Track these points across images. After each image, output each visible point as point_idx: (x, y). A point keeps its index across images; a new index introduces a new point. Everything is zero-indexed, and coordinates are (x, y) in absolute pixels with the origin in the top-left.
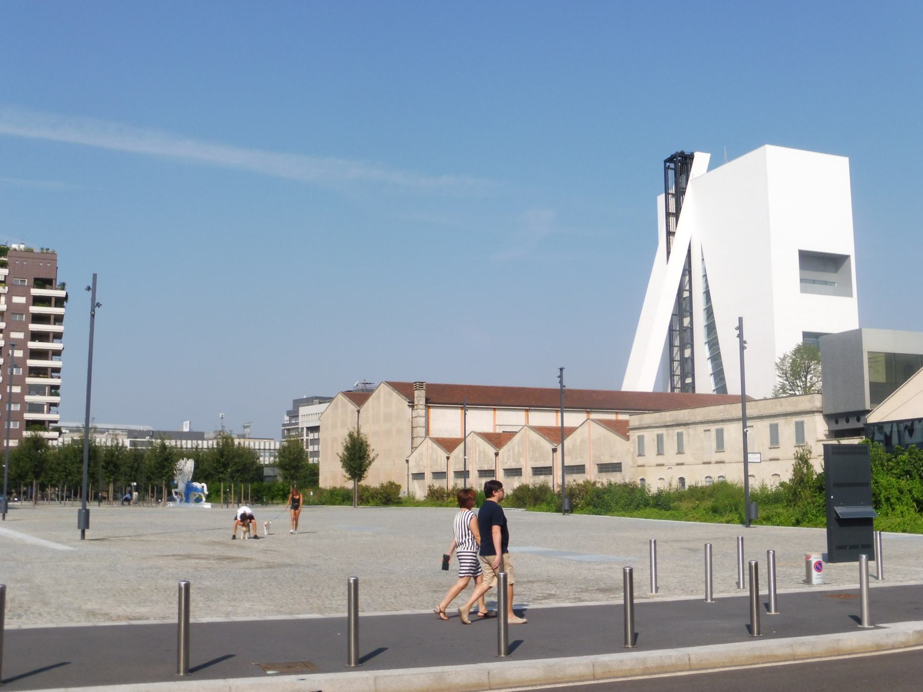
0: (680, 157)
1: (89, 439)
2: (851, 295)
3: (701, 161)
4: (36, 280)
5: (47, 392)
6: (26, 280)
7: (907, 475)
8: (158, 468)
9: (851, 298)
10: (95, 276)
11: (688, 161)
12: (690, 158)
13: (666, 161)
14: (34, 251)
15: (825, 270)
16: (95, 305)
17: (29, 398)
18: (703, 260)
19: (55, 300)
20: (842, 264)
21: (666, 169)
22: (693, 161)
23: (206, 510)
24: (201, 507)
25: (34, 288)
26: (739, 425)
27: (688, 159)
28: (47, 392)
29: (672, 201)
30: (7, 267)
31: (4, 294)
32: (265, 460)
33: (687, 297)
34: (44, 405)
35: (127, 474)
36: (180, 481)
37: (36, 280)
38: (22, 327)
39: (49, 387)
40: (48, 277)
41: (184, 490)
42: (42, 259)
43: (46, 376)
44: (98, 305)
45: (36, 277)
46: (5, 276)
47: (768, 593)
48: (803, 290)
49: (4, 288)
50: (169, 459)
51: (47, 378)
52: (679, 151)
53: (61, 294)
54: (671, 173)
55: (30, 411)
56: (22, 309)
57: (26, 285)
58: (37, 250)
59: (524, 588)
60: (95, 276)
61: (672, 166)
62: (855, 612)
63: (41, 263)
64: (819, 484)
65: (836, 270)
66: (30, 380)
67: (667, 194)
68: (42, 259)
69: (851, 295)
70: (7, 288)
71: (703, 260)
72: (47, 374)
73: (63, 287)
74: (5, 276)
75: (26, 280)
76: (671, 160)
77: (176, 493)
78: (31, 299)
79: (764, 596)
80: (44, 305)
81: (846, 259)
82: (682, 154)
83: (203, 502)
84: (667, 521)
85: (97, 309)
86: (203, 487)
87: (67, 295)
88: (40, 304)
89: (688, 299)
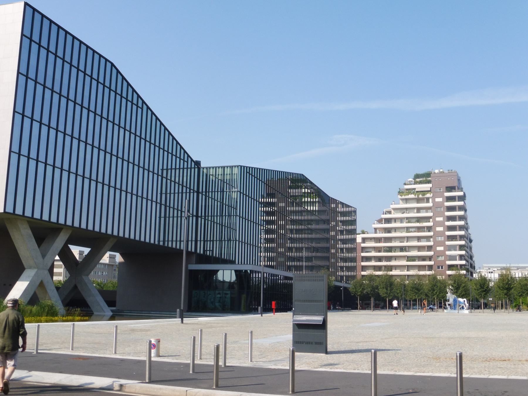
4: (447, 187)
5: (457, 249)
6: (442, 188)
7: (450, 280)
8: (430, 290)
14: (444, 172)
17: (448, 253)
19: (458, 197)
23: (466, 315)
24: (463, 312)
25: (446, 192)
28: (457, 249)
30: (431, 183)
31: (431, 197)
32: (492, 284)
34: (457, 256)
36: (450, 298)
37: (447, 187)
38: (441, 215)
39: (459, 246)
40: (453, 186)
41: (453, 302)
42: (448, 176)
43: (456, 240)
45: (446, 186)
46: (431, 188)
47: (456, 376)
48: (200, 161)
49: (431, 195)
50: (436, 285)
51: (457, 241)
53: (461, 194)
55: (450, 260)
56: (440, 205)
57: (442, 191)
58: (446, 172)
63: (453, 178)
64: (354, 290)
66: (448, 243)
68: (448, 176)
70: (432, 194)
72: (457, 239)
73: (461, 189)
74: (431, 188)
75: (442, 188)
77: (449, 305)
78: (445, 198)
80: (453, 201)
83: (465, 310)
86: (464, 301)
87: (464, 193)
88: (450, 201)
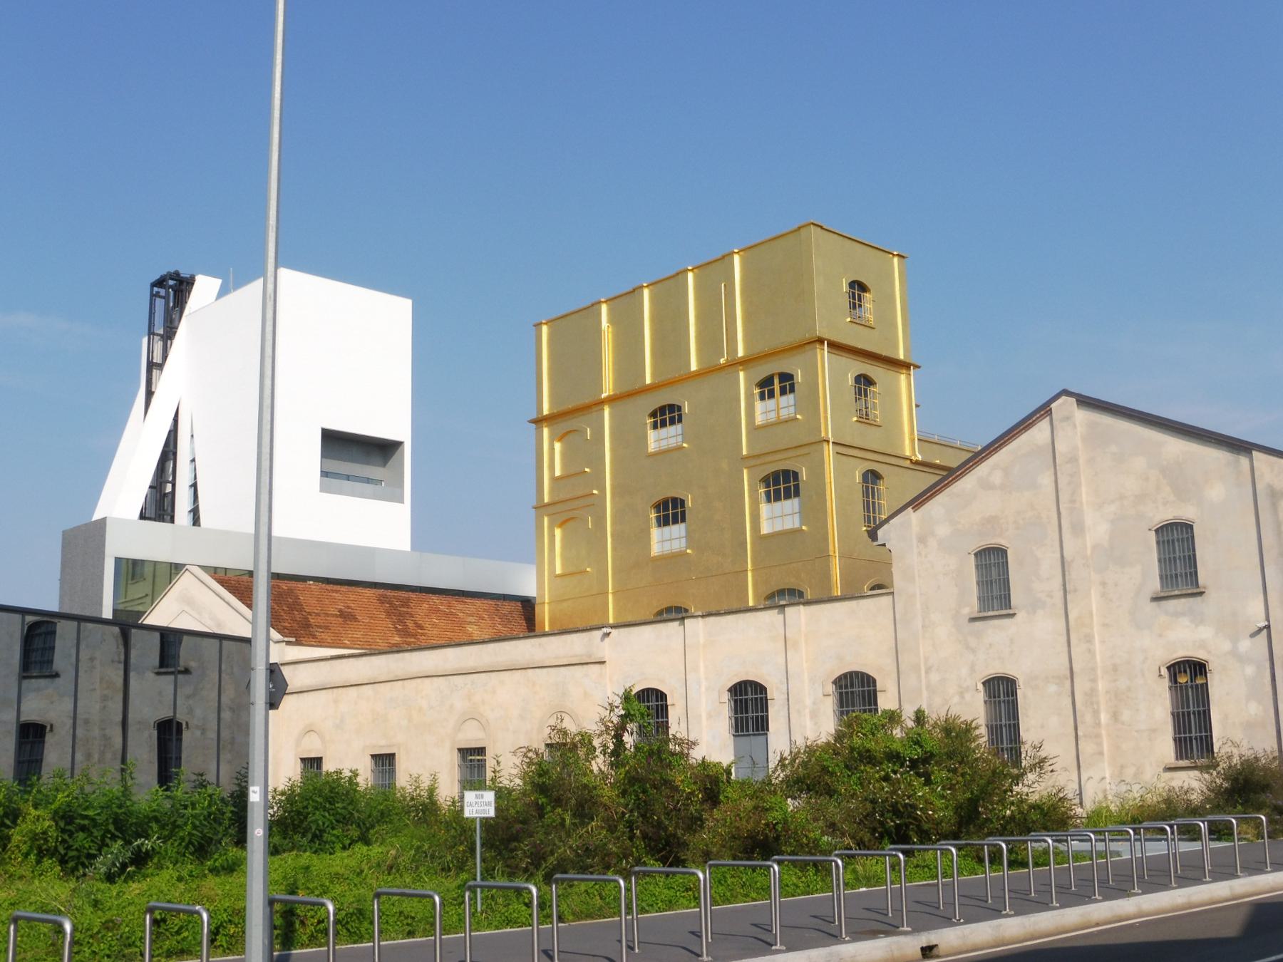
0: (172, 279)
1: (480, 806)
2: (401, 500)
3: (204, 289)
9: (402, 505)
11: (184, 287)
12: (188, 283)
13: (154, 285)
18: (192, 436)
21: (153, 296)
22: (192, 288)
27: (185, 284)
29: (158, 346)
33: (169, 493)
35: (58, 814)
48: (324, 489)
54: (160, 303)
61: (162, 292)
62: (696, 929)
65: (384, 463)
67: (151, 333)
69: (401, 500)
71: (192, 436)
76: (160, 283)
79: (1138, 858)
81: (397, 449)
82: (176, 276)
84: (1187, 850)
89: (170, 496)
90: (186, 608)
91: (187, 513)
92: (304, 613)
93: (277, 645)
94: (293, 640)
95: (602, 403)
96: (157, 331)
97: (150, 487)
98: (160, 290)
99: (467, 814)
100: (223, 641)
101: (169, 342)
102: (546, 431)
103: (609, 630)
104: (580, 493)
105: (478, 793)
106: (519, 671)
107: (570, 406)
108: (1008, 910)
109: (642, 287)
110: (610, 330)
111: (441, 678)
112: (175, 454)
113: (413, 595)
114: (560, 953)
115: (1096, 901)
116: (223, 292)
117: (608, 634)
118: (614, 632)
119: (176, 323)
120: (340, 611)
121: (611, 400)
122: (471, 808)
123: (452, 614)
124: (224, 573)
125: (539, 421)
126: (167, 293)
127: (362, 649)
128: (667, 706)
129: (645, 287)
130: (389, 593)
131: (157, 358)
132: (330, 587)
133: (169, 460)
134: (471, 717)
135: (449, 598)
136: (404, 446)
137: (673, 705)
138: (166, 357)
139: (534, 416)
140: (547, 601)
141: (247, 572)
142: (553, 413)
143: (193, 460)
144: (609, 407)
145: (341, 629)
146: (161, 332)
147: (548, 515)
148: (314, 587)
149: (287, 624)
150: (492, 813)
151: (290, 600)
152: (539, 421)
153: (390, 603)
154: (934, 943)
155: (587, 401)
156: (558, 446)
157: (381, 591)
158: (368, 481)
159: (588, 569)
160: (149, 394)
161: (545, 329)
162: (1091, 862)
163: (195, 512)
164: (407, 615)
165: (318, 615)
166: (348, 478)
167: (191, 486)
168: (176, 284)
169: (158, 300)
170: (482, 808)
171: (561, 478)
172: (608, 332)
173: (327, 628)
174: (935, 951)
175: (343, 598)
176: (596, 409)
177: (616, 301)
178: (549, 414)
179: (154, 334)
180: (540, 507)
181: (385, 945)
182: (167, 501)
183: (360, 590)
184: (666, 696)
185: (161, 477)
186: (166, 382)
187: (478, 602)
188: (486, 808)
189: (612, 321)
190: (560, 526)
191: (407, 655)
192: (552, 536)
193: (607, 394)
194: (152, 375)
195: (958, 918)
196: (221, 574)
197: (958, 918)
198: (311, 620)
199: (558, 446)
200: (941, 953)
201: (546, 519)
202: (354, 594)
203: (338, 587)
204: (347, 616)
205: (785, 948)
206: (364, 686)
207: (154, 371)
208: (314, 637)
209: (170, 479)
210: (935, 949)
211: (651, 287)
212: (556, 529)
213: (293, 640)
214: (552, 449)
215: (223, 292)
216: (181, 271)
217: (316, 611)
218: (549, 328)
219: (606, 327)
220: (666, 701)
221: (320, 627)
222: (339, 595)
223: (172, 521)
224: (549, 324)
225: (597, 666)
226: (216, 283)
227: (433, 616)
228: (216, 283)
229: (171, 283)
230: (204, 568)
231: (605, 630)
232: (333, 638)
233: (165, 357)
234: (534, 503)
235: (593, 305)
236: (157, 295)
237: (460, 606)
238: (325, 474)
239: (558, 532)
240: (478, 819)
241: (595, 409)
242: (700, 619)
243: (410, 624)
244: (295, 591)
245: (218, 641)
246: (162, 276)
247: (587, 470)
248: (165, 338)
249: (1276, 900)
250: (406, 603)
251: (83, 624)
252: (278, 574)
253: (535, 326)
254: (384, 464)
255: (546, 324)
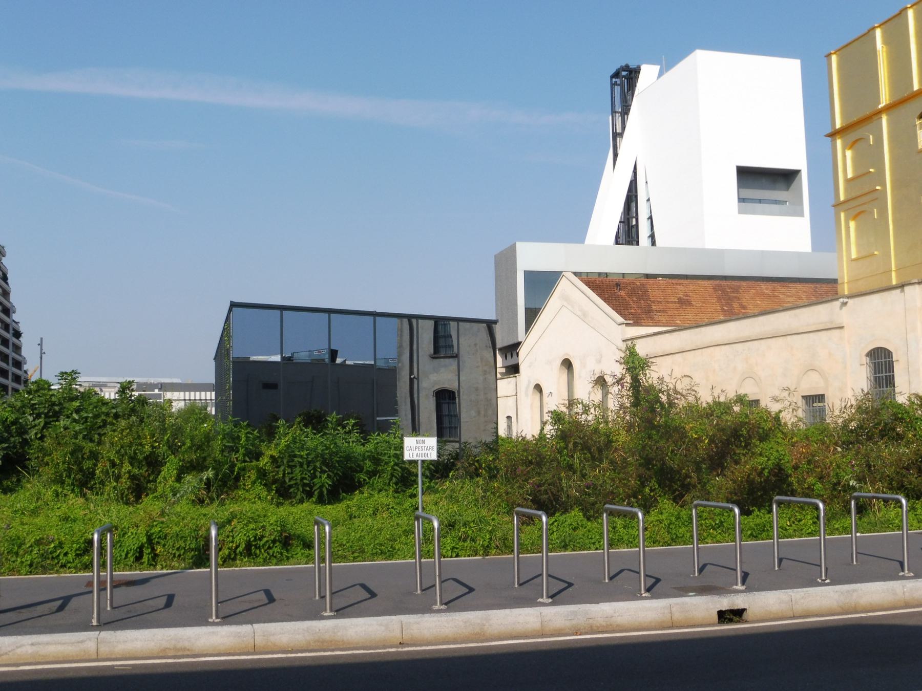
0: (624, 71)
2: (801, 214)
3: (648, 74)
10: (42, 339)
13: (612, 77)
15: (774, 189)
16: (42, 353)
18: (647, 182)
20: (794, 180)
21: (613, 85)
26: (183, 398)
27: (633, 73)
44: (44, 353)
48: (740, 212)
52: (624, 65)
54: (617, 89)
59: (267, 463)
60: (42, 339)
61: (618, 81)
65: (788, 188)
67: (613, 112)
69: (801, 214)
71: (647, 182)
76: (616, 75)
82: (626, 68)
85: (40, 343)
90: (565, 304)
91: (647, 238)
92: (649, 302)
93: (620, 326)
94: (631, 322)
95: (880, 112)
96: (617, 110)
97: (620, 222)
98: (617, 80)
99: (407, 456)
100: (419, 320)
101: (626, 116)
102: (839, 143)
103: (845, 300)
104: (866, 190)
105: (419, 439)
106: (781, 338)
107: (855, 119)
108: (906, 572)
109: (906, 8)
110: (884, 49)
111: (727, 346)
112: (636, 197)
113: (744, 284)
114: (858, 555)
115: (904, 578)
116: (661, 74)
117: (845, 304)
118: (851, 301)
119: (630, 103)
120: (680, 299)
121: (888, 108)
122: (411, 452)
123: (774, 296)
124: (622, 276)
125: (833, 135)
126: (622, 82)
127: (670, 326)
128: (893, 362)
129: (910, 7)
130: (724, 283)
131: (619, 130)
132: (674, 281)
133: (632, 202)
134: (749, 376)
135: (775, 284)
136: (801, 176)
137: (898, 361)
138: (625, 127)
139: (829, 130)
140: (846, 281)
141: (641, 275)
142: (844, 126)
143: (648, 200)
144: (886, 115)
145: (676, 312)
146: (620, 110)
147: (844, 211)
148: (662, 282)
149: (633, 311)
150: (434, 456)
151: (640, 293)
152: (833, 135)
153: (723, 291)
154: (741, 606)
155: (868, 112)
156: (849, 153)
157: (717, 282)
158: (776, 202)
159: (876, 253)
160: (616, 155)
161: (834, 58)
162: (313, 565)
163: (652, 237)
164: (735, 299)
165: (660, 302)
166: (760, 201)
167: (648, 219)
168: (627, 74)
169: (616, 87)
170: (424, 452)
171: (852, 179)
172: (883, 52)
173: (665, 312)
174: (745, 616)
175: (681, 290)
176: (876, 118)
177: (888, 24)
178: (841, 127)
179: (616, 112)
180: (838, 205)
181: (613, 552)
182: (634, 230)
183: (700, 282)
184: (892, 353)
185: (628, 214)
186: (625, 145)
187: (799, 286)
188: (428, 452)
189: (886, 42)
190: (855, 218)
191: (703, 329)
192: (848, 228)
193: (884, 104)
194: (616, 142)
195: (824, 578)
196: (584, 276)
197: (824, 578)
198: (653, 307)
199: (849, 153)
200: (749, 619)
201: (842, 215)
202: (692, 286)
203: (682, 281)
204: (684, 302)
205: (912, 574)
206: (676, 355)
207: (618, 139)
208: (652, 319)
209: (634, 215)
210: (745, 613)
211: (914, 7)
212: (850, 221)
213: (631, 322)
214: (844, 156)
215: (661, 74)
216: (630, 64)
217: (659, 300)
218: (838, 56)
219: (881, 47)
220: (892, 358)
221: (659, 312)
222: (681, 286)
223: (638, 244)
224: (837, 53)
225: (838, 331)
226: (657, 68)
227: (757, 299)
228: (657, 68)
229: (624, 73)
230: (575, 274)
231: (841, 300)
232: (668, 319)
233: (624, 128)
234: (833, 202)
235: (869, 31)
236: (616, 84)
237: (783, 290)
238: (741, 200)
239: (852, 224)
240: (419, 462)
241: (875, 118)
242: (917, 286)
243: (736, 305)
244: (646, 286)
245: (373, 317)
246: (617, 70)
247: (872, 170)
248: (623, 113)
249: (884, 622)
250: (736, 290)
251: (284, 312)
252: (647, 275)
253: (826, 57)
254: (787, 188)
255: (835, 53)
